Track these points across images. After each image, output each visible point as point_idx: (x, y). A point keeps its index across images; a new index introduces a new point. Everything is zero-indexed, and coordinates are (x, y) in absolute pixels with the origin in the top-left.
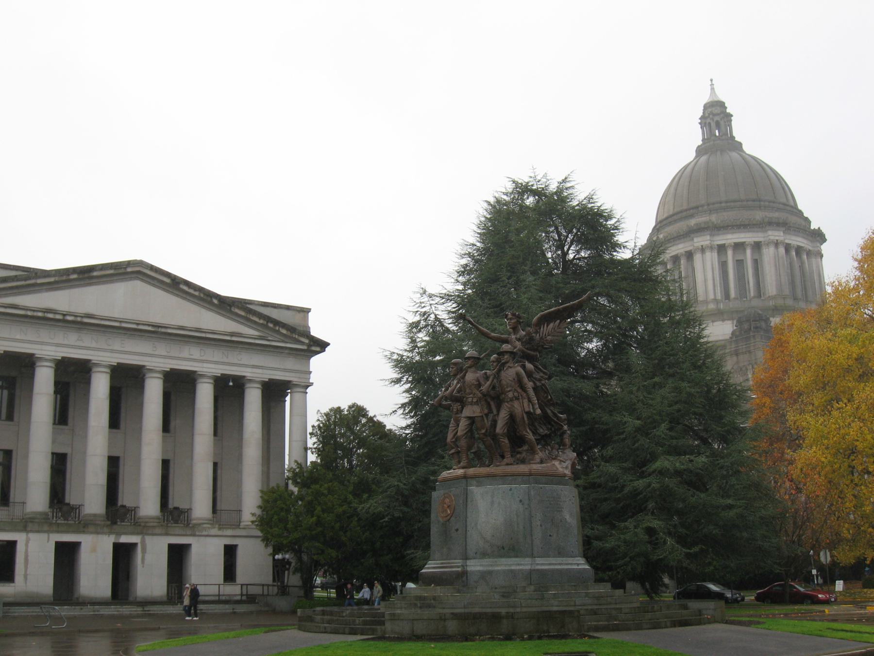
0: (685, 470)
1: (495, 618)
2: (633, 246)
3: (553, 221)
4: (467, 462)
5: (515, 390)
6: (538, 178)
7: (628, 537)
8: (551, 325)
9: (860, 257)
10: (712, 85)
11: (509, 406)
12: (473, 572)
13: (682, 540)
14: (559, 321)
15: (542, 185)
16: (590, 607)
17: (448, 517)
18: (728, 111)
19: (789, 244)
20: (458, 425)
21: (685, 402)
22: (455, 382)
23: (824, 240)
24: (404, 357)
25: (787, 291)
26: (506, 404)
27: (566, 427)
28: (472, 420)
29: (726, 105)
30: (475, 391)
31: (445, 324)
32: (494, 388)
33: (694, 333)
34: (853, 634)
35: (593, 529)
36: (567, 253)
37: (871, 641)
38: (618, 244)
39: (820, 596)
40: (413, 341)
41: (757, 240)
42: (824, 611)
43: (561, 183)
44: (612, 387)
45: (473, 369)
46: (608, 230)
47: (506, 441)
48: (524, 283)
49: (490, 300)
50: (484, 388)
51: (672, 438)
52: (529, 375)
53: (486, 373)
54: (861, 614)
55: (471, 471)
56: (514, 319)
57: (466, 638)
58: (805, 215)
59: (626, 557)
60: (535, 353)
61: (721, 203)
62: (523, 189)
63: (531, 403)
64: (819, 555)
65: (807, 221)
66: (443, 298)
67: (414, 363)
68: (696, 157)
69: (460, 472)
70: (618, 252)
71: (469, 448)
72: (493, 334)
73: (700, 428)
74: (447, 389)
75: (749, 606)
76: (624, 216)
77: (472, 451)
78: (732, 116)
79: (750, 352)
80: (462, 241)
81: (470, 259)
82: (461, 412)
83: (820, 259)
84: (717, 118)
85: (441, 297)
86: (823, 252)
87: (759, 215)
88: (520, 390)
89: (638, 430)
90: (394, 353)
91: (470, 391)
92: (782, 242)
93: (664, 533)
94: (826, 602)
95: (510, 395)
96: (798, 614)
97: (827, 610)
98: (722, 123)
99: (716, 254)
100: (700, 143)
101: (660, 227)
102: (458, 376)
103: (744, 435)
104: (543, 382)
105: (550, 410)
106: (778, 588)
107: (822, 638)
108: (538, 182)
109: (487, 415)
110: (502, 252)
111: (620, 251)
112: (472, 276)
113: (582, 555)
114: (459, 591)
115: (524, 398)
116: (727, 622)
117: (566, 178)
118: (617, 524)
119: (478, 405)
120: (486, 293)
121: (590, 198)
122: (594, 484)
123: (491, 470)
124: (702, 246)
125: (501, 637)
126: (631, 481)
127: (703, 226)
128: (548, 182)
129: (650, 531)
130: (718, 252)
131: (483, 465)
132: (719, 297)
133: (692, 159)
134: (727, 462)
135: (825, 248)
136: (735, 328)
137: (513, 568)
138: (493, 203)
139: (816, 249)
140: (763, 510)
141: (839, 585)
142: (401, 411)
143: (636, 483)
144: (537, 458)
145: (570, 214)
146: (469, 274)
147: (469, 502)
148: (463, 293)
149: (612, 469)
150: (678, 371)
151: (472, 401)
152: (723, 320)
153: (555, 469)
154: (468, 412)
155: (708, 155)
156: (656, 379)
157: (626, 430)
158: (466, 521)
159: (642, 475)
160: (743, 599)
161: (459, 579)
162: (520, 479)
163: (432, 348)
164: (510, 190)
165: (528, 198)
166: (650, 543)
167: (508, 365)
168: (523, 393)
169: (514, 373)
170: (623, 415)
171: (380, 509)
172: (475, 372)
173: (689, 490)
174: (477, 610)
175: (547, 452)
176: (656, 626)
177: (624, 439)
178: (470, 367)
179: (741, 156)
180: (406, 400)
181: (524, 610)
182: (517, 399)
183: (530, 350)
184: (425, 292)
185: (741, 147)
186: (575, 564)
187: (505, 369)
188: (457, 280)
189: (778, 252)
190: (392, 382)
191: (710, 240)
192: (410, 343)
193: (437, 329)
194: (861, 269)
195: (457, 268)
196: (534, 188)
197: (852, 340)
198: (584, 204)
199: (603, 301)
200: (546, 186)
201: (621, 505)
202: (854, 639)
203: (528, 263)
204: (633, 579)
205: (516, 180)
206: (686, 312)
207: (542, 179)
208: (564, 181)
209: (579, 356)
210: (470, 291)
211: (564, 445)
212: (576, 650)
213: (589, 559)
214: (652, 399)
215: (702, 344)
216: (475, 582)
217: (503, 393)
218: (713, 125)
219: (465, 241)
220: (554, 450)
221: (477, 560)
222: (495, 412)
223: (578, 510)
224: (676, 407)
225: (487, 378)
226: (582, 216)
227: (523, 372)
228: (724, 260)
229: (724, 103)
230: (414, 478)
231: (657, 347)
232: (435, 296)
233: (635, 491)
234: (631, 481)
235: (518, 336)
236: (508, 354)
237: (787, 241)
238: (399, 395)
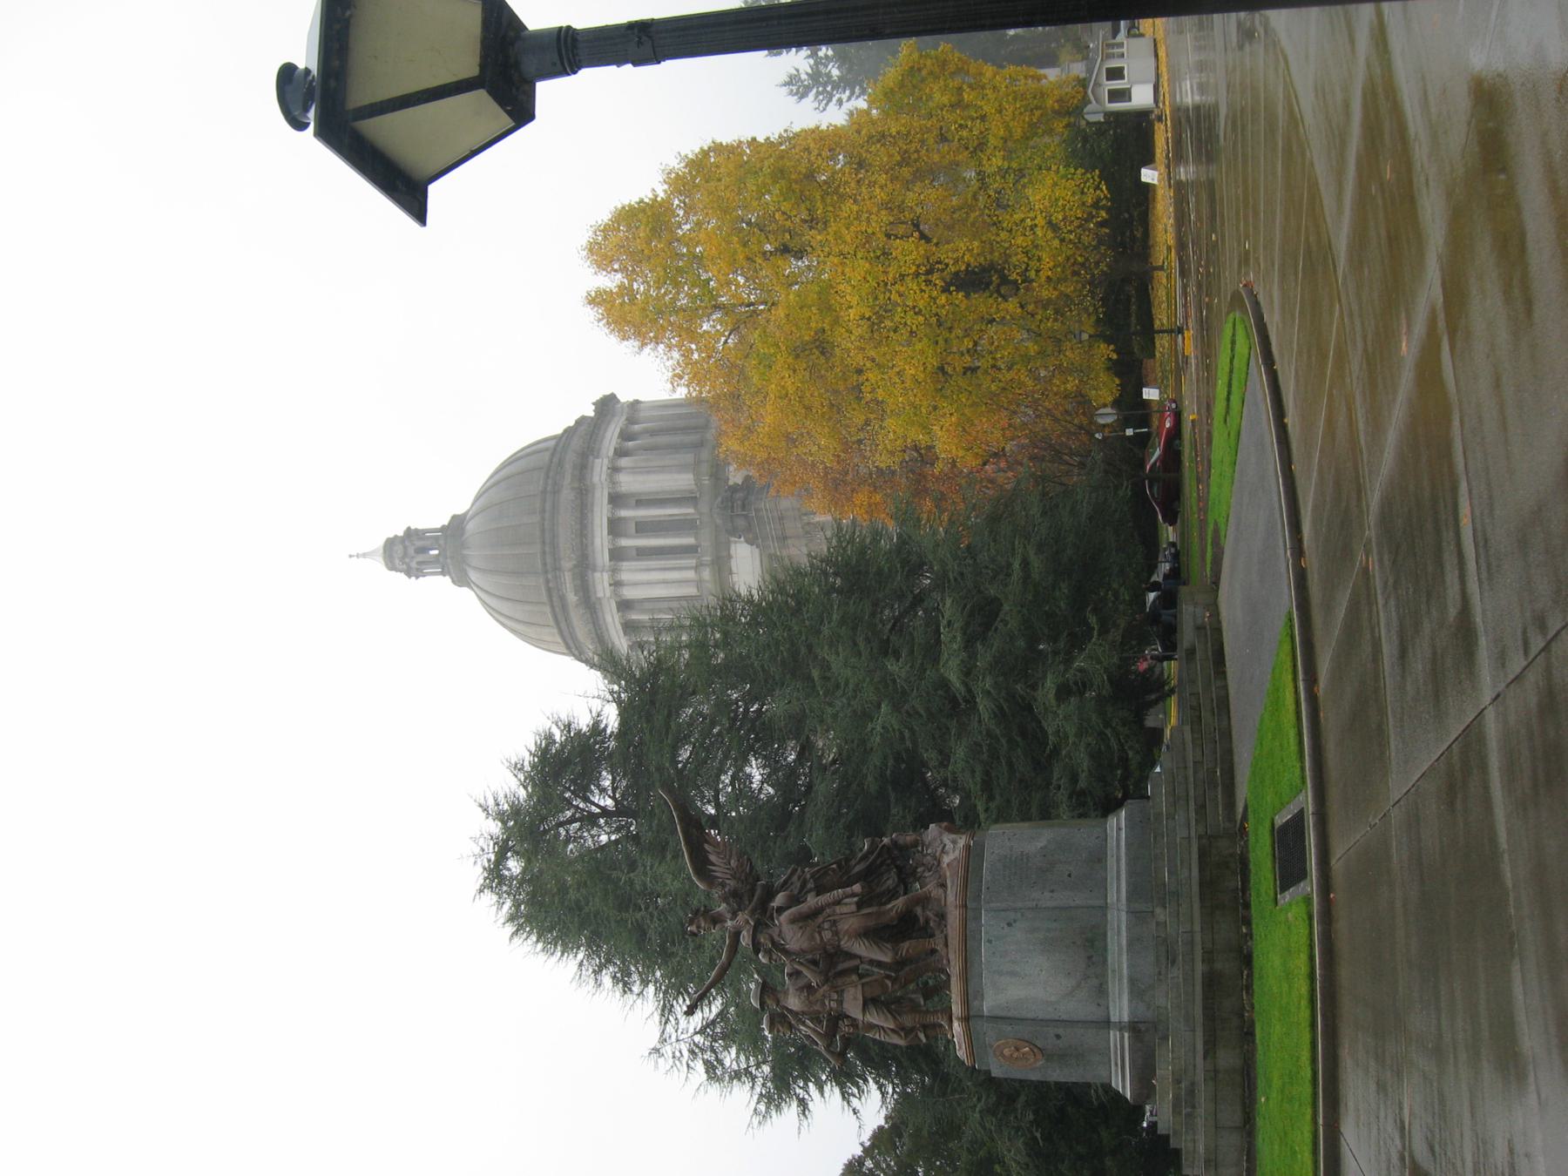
0: (965, 634)
1: (1212, 982)
2: (599, 701)
3: (550, 830)
5: (819, 927)
6: (477, 850)
7: (1071, 730)
8: (713, 858)
9: (637, 344)
10: (358, 556)
11: (846, 938)
12: (1131, 1013)
13: (1077, 641)
15: (488, 845)
16: (1193, 814)
17: (1036, 1050)
18: (401, 534)
21: (854, 629)
24: (764, 1092)
25: (689, 458)
26: (842, 943)
27: (886, 840)
28: (869, 1002)
30: (818, 995)
31: (712, 1017)
32: (815, 963)
33: (744, 609)
34: (1235, 383)
35: (1059, 787)
36: (604, 809)
37: (1247, 356)
38: (593, 725)
39: (1168, 425)
40: (737, 1075)
41: (606, 500)
42: (1193, 421)
43: (488, 814)
44: (827, 745)
45: (781, 996)
46: (569, 740)
47: (906, 945)
48: (649, 885)
49: (673, 944)
51: (912, 652)
52: (795, 900)
53: (790, 975)
54: (1197, 365)
55: (957, 1009)
57: (1248, 1034)
58: (572, 423)
59: (1106, 735)
61: (544, 553)
62: (495, 877)
63: (843, 899)
64: (1104, 426)
65: (582, 421)
66: (668, 1019)
67: (775, 1075)
68: (469, 586)
69: (957, 1027)
70: (606, 726)
71: (915, 1008)
73: (896, 606)
75: (1183, 535)
76: (549, 714)
77: (922, 1003)
78: (409, 528)
79: (781, 518)
80: (574, 983)
81: (604, 971)
82: (855, 1020)
84: (411, 551)
85: (666, 1023)
86: (631, 400)
87: (567, 495)
88: (820, 919)
89: (896, 708)
90: (755, 1109)
91: (819, 1003)
92: (612, 461)
93: (1066, 670)
94: (1178, 416)
95: (827, 935)
96: (1197, 463)
97: (1189, 416)
98: (420, 543)
99: (625, 564)
100: (447, 579)
101: (577, 648)
103: (910, 537)
104: (808, 876)
106: (1155, 489)
107: (1243, 432)
108: (483, 850)
110: (595, 916)
111: (604, 722)
112: (633, 969)
113: (1102, 820)
114: (1165, 1038)
115: (834, 911)
116: (1216, 583)
117: (481, 806)
118: (1051, 746)
119: (843, 991)
120: (662, 946)
121: (517, 767)
122: (983, 781)
123: (955, 970)
124: (610, 585)
125: (1246, 972)
126: (980, 721)
127: (578, 582)
128: (486, 835)
129: (1063, 692)
130: (623, 560)
131: (947, 984)
132: (693, 562)
133: (473, 593)
134: (953, 566)
135: (624, 397)
136: (742, 539)
137: (1124, 942)
138: (515, 929)
139: (626, 410)
140: (1031, 512)
141: (1150, 394)
142: (855, 1102)
143: (985, 716)
144: (936, 892)
145: (538, 800)
146: (629, 975)
147: (1010, 1015)
148: (661, 985)
149: (960, 752)
150: (804, 638)
151: (837, 1001)
152: (730, 557)
153: (955, 863)
154: (853, 1008)
155: (468, 569)
156: (815, 674)
157: (896, 727)
158: (1042, 1020)
159: (971, 700)
160: (1173, 545)
161: (1143, 1033)
162: (971, 925)
163: (750, 1042)
164: (495, 898)
165: (509, 869)
166: (1082, 694)
167: (776, 938)
168: (824, 914)
170: (871, 731)
171: (1020, 1143)
172: (786, 993)
173: (996, 629)
174: (1198, 1011)
175: (926, 874)
176: (1223, 705)
177: (911, 730)
178: (778, 1003)
179: (472, 518)
180: (837, 1090)
181: (1197, 928)
182: (834, 923)
183: (753, 896)
184: (656, 1050)
185: (458, 516)
188: (638, 995)
189: (625, 468)
190: (804, 1114)
191: (602, 571)
192: (740, 1080)
193: (722, 1032)
194: (657, 340)
195: (618, 994)
196: (493, 857)
197: (767, 364)
198: (526, 779)
199: (685, 754)
200: (492, 838)
201: (1019, 739)
202: (1243, 381)
203: (615, 874)
204: (1139, 719)
205: (478, 887)
206: (708, 621)
207: (480, 844)
209: (773, 797)
210: (658, 974)
211: (915, 844)
212: (1268, 849)
213: (1109, 807)
214: (847, 684)
215: (762, 598)
216: (1148, 1009)
217: (825, 949)
218: (420, 558)
219: (574, 978)
221: (1111, 1004)
222: (857, 962)
223: (1026, 824)
224: (862, 645)
226: (544, 783)
227: (787, 913)
228: (634, 553)
230: (969, 1084)
231: (764, 670)
232: (663, 1032)
233: (996, 716)
234: (980, 721)
235: (729, 916)
237: (611, 453)
238: (827, 1103)
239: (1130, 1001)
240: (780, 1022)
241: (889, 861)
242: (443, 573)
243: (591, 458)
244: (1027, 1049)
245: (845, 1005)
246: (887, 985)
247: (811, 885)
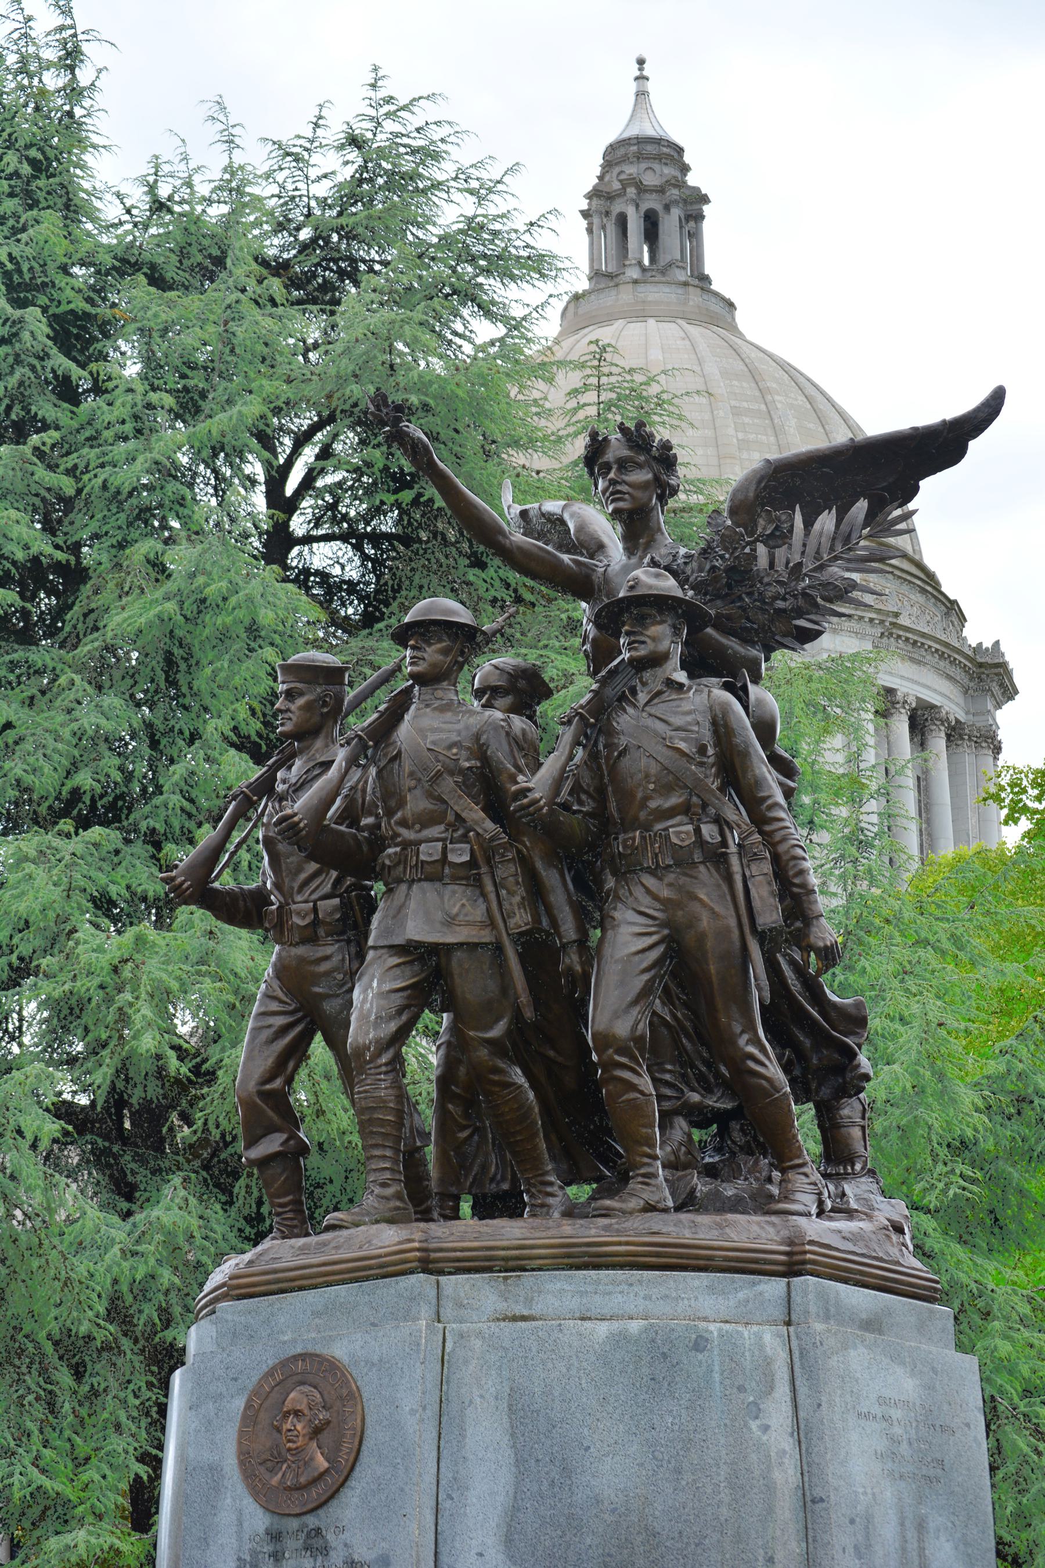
10: (641, 78)
11: (665, 893)
18: (692, 179)
23: (1009, 692)
26: (649, 881)
29: (687, 158)
56: (640, 466)
68: (561, 334)
78: (705, 199)
83: (991, 759)
84: (652, 202)
86: (1001, 735)
115: (756, 858)
119: (477, 883)
151: (444, 860)
229: (680, 150)
244: (322, 1463)
246: (489, 1027)
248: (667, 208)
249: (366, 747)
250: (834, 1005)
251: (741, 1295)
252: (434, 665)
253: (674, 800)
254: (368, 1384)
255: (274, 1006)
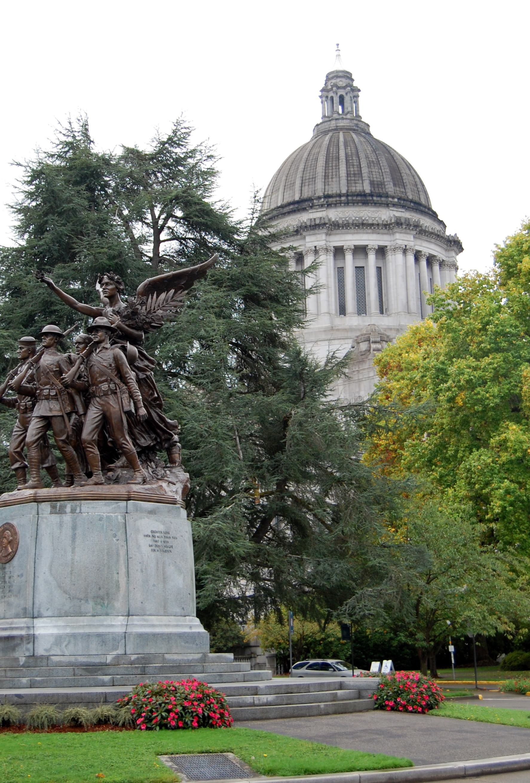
4: (38, 481)
5: (111, 380)
8: (163, 296)
11: (102, 402)
12: (45, 635)
14: (173, 291)
17: (9, 557)
18: (355, 84)
19: (420, 252)
20: (26, 430)
22: (25, 367)
26: (98, 399)
29: (353, 77)
41: (382, 243)
50: (67, 376)
52: (131, 360)
53: (69, 357)
55: (44, 492)
56: (111, 284)
60: (139, 333)
63: (133, 399)
68: (315, 137)
72: (80, 304)
74: (12, 378)
77: (45, 466)
82: (32, 410)
84: (341, 92)
88: (118, 381)
91: (46, 380)
95: (104, 387)
98: (347, 99)
99: (332, 258)
102: (30, 360)
104: (148, 373)
105: (156, 412)
109: (69, 415)
115: (124, 393)
124: (315, 247)
127: (318, 222)
130: (335, 256)
133: (308, 140)
139: (451, 260)
151: (49, 395)
167: (103, 345)
168: (122, 384)
169: (111, 356)
186: (186, 626)
187: (98, 350)
191: (325, 240)
208: (178, 123)
211: (172, 461)
217: (93, 385)
218: (336, 100)
220: (159, 469)
225: (71, 362)
228: (340, 265)
229: (351, 74)
235: (116, 308)
236: (104, 331)
239: (52, 635)
240: (29, 350)
241: (159, 440)
242: (324, 116)
243: (414, 232)
244: (10, 550)
245: (45, 402)
246: (61, 436)
247: (142, 376)
248: (347, 94)
249: (33, 365)
250: (169, 423)
251: (113, 506)
252: (48, 343)
253: (103, 379)
254: (19, 530)
255: (18, 429)
